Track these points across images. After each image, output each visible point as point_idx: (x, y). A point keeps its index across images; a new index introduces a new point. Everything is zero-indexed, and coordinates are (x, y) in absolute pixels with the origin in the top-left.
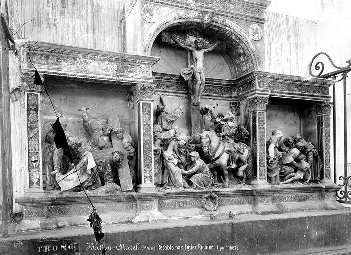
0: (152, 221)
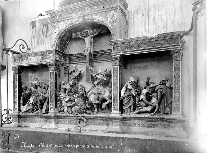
0: (49, 129)
